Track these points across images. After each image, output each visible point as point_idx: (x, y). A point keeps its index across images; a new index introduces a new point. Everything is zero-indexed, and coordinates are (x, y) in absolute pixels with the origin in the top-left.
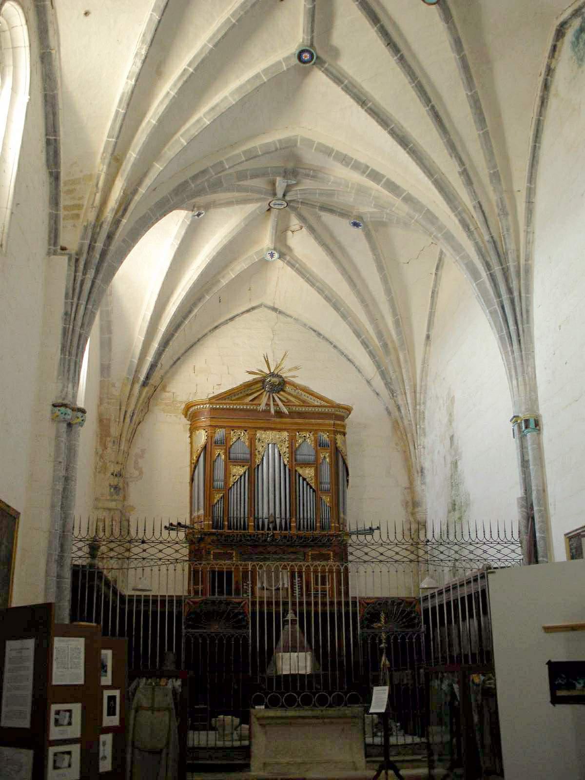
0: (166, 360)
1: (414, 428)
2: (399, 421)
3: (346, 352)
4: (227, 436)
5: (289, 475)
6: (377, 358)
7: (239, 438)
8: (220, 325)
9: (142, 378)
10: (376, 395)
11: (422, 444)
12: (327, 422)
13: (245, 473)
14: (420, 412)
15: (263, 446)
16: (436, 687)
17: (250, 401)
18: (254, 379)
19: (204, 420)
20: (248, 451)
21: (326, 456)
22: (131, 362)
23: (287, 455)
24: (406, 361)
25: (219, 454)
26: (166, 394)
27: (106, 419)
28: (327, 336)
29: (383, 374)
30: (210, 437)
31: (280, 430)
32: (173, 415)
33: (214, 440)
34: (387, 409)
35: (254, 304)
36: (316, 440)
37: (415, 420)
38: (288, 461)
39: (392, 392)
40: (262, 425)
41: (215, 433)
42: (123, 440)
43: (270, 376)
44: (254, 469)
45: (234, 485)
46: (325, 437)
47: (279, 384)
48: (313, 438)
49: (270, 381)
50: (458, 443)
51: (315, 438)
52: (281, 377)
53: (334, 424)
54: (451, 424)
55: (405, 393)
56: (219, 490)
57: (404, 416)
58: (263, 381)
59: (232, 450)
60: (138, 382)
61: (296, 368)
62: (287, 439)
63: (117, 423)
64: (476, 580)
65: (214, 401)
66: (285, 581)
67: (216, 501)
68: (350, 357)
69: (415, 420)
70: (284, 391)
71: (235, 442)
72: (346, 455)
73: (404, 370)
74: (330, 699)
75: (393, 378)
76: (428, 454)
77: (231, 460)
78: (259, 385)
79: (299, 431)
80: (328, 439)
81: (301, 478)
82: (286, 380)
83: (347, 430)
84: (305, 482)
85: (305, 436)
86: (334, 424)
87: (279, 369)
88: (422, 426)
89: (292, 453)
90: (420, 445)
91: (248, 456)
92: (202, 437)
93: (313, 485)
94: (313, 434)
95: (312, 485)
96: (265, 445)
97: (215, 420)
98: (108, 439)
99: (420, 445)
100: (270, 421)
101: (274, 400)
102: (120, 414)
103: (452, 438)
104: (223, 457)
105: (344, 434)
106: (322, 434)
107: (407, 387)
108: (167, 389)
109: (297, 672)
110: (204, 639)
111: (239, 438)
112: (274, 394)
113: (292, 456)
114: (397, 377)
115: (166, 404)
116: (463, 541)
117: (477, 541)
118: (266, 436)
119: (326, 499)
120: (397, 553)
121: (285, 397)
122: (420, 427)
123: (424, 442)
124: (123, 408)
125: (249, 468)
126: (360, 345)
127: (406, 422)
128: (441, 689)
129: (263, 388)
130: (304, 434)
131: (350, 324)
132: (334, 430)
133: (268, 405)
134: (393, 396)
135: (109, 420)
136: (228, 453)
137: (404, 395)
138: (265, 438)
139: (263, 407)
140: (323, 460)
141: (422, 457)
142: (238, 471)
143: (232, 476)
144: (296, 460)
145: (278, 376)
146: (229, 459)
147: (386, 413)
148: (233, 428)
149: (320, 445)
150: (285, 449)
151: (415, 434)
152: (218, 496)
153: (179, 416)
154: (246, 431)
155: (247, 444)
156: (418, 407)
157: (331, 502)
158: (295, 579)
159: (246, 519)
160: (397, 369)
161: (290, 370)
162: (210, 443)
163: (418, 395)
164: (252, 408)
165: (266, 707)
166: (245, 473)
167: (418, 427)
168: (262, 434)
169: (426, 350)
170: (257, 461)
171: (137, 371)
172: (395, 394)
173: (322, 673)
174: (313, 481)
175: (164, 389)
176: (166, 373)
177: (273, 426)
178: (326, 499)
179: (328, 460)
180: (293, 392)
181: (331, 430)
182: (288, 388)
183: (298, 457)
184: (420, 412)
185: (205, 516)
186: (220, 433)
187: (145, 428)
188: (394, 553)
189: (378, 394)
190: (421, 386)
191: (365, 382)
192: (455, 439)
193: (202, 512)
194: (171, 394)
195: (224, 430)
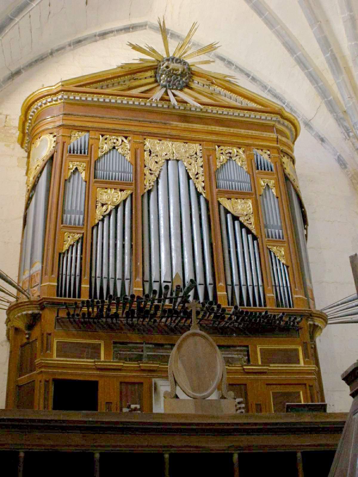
3: (270, 85)
4: (91, 142)
7: (114, 148)
8: (85, 39)
12: (265, 134)
15: (156, 162)
25: (76, 169)
31: (186, 140)
33: (67, 147)
35: (135, 21)
36: (250, 159)
40: (156, 131)
41: (70, 137)
44: (143, 196)
45: (103, 220)
46: (264, 157)
47: (183, 75)
49: (167, 67)
51: (247, 157)
52: (185, 63)
56: (73, 228)
58: (155, 68)
67: (66, 247)
70: (191, 88)
78: (151, 73)
79: (220, 144)
80: (269, 161)
81: (229, 216)
82: (193, 68)
84: (236, 223)
87: (182, 52)
91: (131, 176)
93: (252, 227)
94: (244, 152)
95: (250, 227)
96: (162, 161)
97: (70, 117)
106: (259, 152)
111: (114, 148)
114: (353, 103)
119: (280, 252)
125: (132, 195)
130: (228, 149)
131: (279, 35)
138: (162, 150)
143: (99, 205)
145: (179, 61)
147: (336, 164)
148: (103, 132)
150: (196, 168)
152: (70, 239)
153: (12, 146)
154: (126, 138)
155: (128, 157)
157: (288, 251)
159: (127, 283)
162: (60, 152)
166: (124, 201)
170: (148, 184)
174: (252, 220)
177: (174, 133)
178: (280, 252)
181: (273, 148)
183: (221, 183)
185: (43, 272)
189: (322, 140)
193: (38, 266)
195: (87, 134)
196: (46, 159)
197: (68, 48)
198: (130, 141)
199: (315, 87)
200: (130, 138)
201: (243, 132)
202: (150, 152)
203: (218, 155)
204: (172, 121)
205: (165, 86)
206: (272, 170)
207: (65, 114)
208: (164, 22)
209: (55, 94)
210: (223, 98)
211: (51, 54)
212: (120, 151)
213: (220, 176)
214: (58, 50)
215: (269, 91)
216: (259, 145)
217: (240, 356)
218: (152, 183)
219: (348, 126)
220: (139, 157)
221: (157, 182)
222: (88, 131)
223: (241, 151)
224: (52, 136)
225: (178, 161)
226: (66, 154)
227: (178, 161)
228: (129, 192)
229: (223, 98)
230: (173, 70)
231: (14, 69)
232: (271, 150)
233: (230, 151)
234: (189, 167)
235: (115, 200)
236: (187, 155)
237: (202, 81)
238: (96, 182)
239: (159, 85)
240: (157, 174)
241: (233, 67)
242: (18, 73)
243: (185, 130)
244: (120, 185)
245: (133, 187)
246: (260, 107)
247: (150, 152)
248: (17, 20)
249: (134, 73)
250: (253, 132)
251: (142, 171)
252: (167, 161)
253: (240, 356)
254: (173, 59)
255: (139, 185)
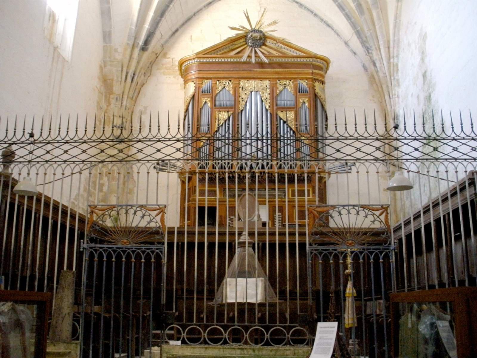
0: (165, 28)
1: (389, 79)
2: (375, 74)
3: (325, 19)
4: (213, 85)
5: (271, 121)
6: (353, 20)
7: (224, 87)
9: (141, 42)
10: (354, 54)
11: (396, 93)
12: (306, 70)
13: (229, 118)
14: (393, 65)
15: (246, 94)
16: (410, 326)
17: (236, 54)
18: (237, 35)
19: (193, 74)
20: (233, 99)
21: (305, 101)
22: (131, 29)
23: (269, 101)
24: (379, 19)
25: (206, 102)
26: (167, 60)
27: (109, 79)
28: (308, 6)
29: (359, 34)
30: (198, 88)
31: (262, 79)
32: (172, 77)
33: (201, 91)
34: (364, 66)
37: (390, 72)
38: (269, 106)
39: (368, 50)
41: (202, 84)
42: (125, 97)
43: (252, 32)
44: (239, 113)
46: (304, 84)
47: (260, 39)
48: (292, 85)
49: (252, 36)
50: (431, 76)
51: (294, 85)
52: (261, 32)
53: (312, 73)
54: (423, 62)
55: (380, 49)
57: (379, 70)
58: (245, 37)
59: (217, 98)
60: (137, 47)
61: (275, 23)
62: (268, 86)
63: (120, 83)
64: (463, 189)
65: (201, 55)
66: (264, 214)
68: (330, 22)
69: (390, 72)
70: (266, 46)
71: (221, 91)
72: (325, 101)
73: (377, 27)
74: (267, 336)
75: (367, 35)
76: (402, 102)
77: (215, 106)
78: (243, 40)
80: (306, 86)
82: (266, 34)
83: (326, 80)
85: (285, 84)
86: (312, 73)
87: (259, 25)
88: (396, 78)
89: (273, 98)
90: (395, 95)
91: (233, 103)
92: (191, 88)
94: (293, 82)
95: (292, 127)
96: (248, 92)
97: (201, 72)
98: (112, 96)
99: (395, 95)
100: (252, 72)
101: (256, 52)
102: (122, 75)
103: (424, 76)
104: (209, 104)
105: (323, 83)
106: (301, 81)
107: (381, 42)
108: (168, 56)
109: (245, 301)
110: (109, 256)
111: (224, 87)
112: (256, 49)
113: (273, 102)
114: (371, 34)
115: (166, 68)
116: (444, 136)
117: (463, 135)
118: (251, 85)
120: (358, 150)
121: (266, 51)
122: (394, 79)
123: (398, 92)
124: (125, 69)
125: (233, 113)
126: (336, 8)
127: (381, 75)
128: (418, 330)
129: (246, 44)
130: (284, 82)
132: (312, 78)
133: (249, 57)
134: (368, 52)
135: (112, 80)
136: (214, 100)
137: (378, 51)
138: (248, 86)
139: (244, 58)
140: (302, 104)
141: (397, 106)
142: (224, 116)
144: (276, 105)
145: (258, 31)
146: (215, 105)
147: (363, 69)
148: (219, 79)
149: (299, 91)
150: (266, 95)
151: (390, 85)
153: (177, 78)
154: (230, 81)
155: (231, 92)
156: (392, 60)
158: (276, 214)
160: (371, 27)
161: (270, 25)
162: (197, 93)
163: (391, 49)
164: (235, 60)
165: (182, 343)
167: (392, 78)
168: (245, 84)
169: (397, 6)
170: (241, 107)
171: (136, 38)
172: (370, 51)
173: (278, 301)
174: (293, 123)
175: (165, 55)
176: (167, 41)
177: (256, 75)
179: (307, 104)
180: (273, 46)
181: (309, 78)
182: (269, 42)
183: (279, 102)
184: (393, 65)
186: (207, 84)
187: (149, 89)
188: (354, 150)
189: (355, 53)
190: (394, 41)
191: (344, 44)
192: (428, 74)
194: (171, 60)
195: (210, 81)
196: (191, 96)
197: (204, 9)
198: (232, 83)
199: (349, 23)
200: (232, 81)
201: (293, 70)
202: (243, 88)
203: (278, 86)
204: (254, 68)
205: (251, 46)
206: (307, 92)
207: (199, 71)
208: (247, 12)
209: (193, 59)
210: (283, 50)
211: (194, 15)
212: (227, 89)
213: (279, 98)
214: (198, 12)
215: (325, 22)
216: (302, 78)
217: (281, 193)
218: (243, 106)
219: (368, 46)
220: (237, 92)
221: (246, 105)
222: (211, 79)
223: (291, 83)
224: (193, 83)
225: (257, 91)
226: (200, 94)
227: (257, 91)
228: (232, 112)
229: (283, 50)
230: (255, 37)
231: (174, 30)
232: (308, 80)
233: (285, 83)
234: (262, 95)
235: (224, 117)
236: (262, 87)
237: (272, 41)
238: (215, 108)
239: (248, 46)
240: (245, 100)
241: (303, 7)
242: (177, 31)
243: (260, 73)
244: (226, 108)
245: (233, 109)
246: (304, 54)
247: (243, 88)
248: (171, 6)
249: (235, 41)
250: (299, 70)
251: (238, 99)
252: (251, 92)
253: (281, 193)
254: (254, 30)
255: (236, 108)
